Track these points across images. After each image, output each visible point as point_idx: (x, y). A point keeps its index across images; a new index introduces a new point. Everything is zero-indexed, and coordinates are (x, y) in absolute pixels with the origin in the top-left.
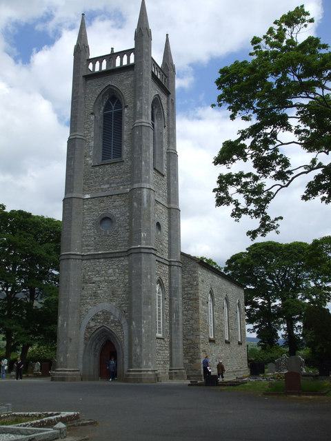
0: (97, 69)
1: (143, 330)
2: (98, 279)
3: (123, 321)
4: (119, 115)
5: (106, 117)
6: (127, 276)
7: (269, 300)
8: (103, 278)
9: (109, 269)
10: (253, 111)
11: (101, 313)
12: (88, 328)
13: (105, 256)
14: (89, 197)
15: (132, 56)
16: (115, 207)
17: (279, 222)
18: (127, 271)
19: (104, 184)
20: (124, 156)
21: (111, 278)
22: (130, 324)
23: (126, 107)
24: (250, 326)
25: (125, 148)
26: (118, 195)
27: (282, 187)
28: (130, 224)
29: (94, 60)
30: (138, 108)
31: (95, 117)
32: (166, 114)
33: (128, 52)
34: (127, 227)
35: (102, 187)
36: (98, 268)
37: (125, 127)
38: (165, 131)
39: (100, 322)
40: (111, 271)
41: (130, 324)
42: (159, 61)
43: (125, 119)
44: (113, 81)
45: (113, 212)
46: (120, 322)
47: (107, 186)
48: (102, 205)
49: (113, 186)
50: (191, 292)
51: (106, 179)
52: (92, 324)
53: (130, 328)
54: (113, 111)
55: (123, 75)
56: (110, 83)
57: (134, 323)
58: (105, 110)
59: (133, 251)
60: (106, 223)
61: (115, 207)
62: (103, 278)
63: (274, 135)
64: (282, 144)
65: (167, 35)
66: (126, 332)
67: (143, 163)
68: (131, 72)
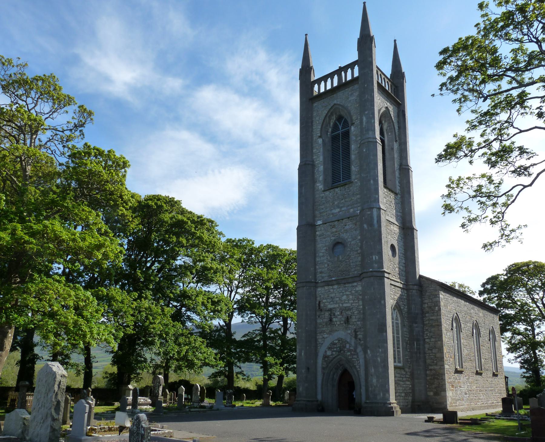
0: (322, 90)
1: (379, 359)
2: (332, 306)
3: (359, 349)
4: (347, 134)
5: (335, 139)
6: (361, 303)
7: (532, 326)
8: (337, 306)
9: (343, 295)
10: (483, 99)
11: (337, 342)
12: (325, 357)
13: (338, 282)
14: (321, 223)
15: (356, 68)
16: (346, 231)
17: (523, 230)
18: (361, 297)
19: (335, 209)
20: (353, 177)
21: (345, 305)
22: (365, 352)
23: (353, 124)
24: (512, 356)
25: (354, 169)
26: (349, 218)
27: (525, 187)
28: (361, 247)
29: (319, 81)
30: (364, 123)
31: (323, 140)
32: (396, 128)
33: (351, 66)
34: (359, 251)
35: (334, 211)
36: (332, 295)
37: (353, 147)
38: (396, 146)
39: (336, 351)
40: (344, 297)
41: (365, 352)
42: (388, 71)
43: (353, 138)
44: (339, 99)
45: (345, 236)
46: (355, 351)
47: (338, 210)
48: (334, 230)
49: (343, 209)
50: (433, 318)
51: (336, 203)
52: (329, 353)
53: (365, 357)
54: (340, 132)
55: (347, 91)
56: (335, 102)
57: (369, 351)
58: (332, 132)
59: (364, 275)
60: (339, 249)
61: (346, 231)
62: (337, 306)
63: (509, 122)
64: (521, 131)
65: (395, 41)
66: (362, 361)
67: (372, 182)
68: (356, 86)
